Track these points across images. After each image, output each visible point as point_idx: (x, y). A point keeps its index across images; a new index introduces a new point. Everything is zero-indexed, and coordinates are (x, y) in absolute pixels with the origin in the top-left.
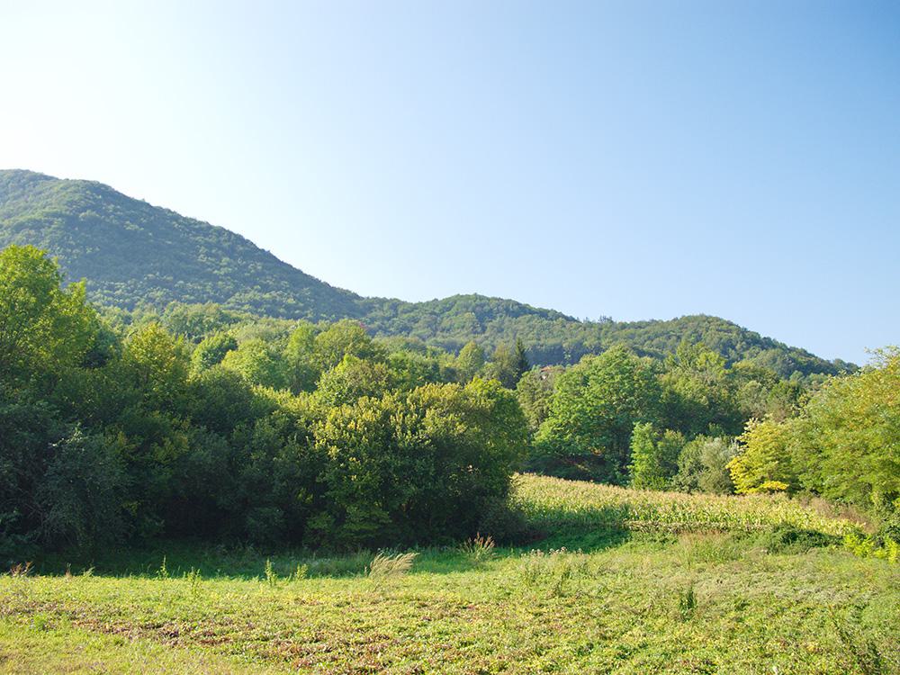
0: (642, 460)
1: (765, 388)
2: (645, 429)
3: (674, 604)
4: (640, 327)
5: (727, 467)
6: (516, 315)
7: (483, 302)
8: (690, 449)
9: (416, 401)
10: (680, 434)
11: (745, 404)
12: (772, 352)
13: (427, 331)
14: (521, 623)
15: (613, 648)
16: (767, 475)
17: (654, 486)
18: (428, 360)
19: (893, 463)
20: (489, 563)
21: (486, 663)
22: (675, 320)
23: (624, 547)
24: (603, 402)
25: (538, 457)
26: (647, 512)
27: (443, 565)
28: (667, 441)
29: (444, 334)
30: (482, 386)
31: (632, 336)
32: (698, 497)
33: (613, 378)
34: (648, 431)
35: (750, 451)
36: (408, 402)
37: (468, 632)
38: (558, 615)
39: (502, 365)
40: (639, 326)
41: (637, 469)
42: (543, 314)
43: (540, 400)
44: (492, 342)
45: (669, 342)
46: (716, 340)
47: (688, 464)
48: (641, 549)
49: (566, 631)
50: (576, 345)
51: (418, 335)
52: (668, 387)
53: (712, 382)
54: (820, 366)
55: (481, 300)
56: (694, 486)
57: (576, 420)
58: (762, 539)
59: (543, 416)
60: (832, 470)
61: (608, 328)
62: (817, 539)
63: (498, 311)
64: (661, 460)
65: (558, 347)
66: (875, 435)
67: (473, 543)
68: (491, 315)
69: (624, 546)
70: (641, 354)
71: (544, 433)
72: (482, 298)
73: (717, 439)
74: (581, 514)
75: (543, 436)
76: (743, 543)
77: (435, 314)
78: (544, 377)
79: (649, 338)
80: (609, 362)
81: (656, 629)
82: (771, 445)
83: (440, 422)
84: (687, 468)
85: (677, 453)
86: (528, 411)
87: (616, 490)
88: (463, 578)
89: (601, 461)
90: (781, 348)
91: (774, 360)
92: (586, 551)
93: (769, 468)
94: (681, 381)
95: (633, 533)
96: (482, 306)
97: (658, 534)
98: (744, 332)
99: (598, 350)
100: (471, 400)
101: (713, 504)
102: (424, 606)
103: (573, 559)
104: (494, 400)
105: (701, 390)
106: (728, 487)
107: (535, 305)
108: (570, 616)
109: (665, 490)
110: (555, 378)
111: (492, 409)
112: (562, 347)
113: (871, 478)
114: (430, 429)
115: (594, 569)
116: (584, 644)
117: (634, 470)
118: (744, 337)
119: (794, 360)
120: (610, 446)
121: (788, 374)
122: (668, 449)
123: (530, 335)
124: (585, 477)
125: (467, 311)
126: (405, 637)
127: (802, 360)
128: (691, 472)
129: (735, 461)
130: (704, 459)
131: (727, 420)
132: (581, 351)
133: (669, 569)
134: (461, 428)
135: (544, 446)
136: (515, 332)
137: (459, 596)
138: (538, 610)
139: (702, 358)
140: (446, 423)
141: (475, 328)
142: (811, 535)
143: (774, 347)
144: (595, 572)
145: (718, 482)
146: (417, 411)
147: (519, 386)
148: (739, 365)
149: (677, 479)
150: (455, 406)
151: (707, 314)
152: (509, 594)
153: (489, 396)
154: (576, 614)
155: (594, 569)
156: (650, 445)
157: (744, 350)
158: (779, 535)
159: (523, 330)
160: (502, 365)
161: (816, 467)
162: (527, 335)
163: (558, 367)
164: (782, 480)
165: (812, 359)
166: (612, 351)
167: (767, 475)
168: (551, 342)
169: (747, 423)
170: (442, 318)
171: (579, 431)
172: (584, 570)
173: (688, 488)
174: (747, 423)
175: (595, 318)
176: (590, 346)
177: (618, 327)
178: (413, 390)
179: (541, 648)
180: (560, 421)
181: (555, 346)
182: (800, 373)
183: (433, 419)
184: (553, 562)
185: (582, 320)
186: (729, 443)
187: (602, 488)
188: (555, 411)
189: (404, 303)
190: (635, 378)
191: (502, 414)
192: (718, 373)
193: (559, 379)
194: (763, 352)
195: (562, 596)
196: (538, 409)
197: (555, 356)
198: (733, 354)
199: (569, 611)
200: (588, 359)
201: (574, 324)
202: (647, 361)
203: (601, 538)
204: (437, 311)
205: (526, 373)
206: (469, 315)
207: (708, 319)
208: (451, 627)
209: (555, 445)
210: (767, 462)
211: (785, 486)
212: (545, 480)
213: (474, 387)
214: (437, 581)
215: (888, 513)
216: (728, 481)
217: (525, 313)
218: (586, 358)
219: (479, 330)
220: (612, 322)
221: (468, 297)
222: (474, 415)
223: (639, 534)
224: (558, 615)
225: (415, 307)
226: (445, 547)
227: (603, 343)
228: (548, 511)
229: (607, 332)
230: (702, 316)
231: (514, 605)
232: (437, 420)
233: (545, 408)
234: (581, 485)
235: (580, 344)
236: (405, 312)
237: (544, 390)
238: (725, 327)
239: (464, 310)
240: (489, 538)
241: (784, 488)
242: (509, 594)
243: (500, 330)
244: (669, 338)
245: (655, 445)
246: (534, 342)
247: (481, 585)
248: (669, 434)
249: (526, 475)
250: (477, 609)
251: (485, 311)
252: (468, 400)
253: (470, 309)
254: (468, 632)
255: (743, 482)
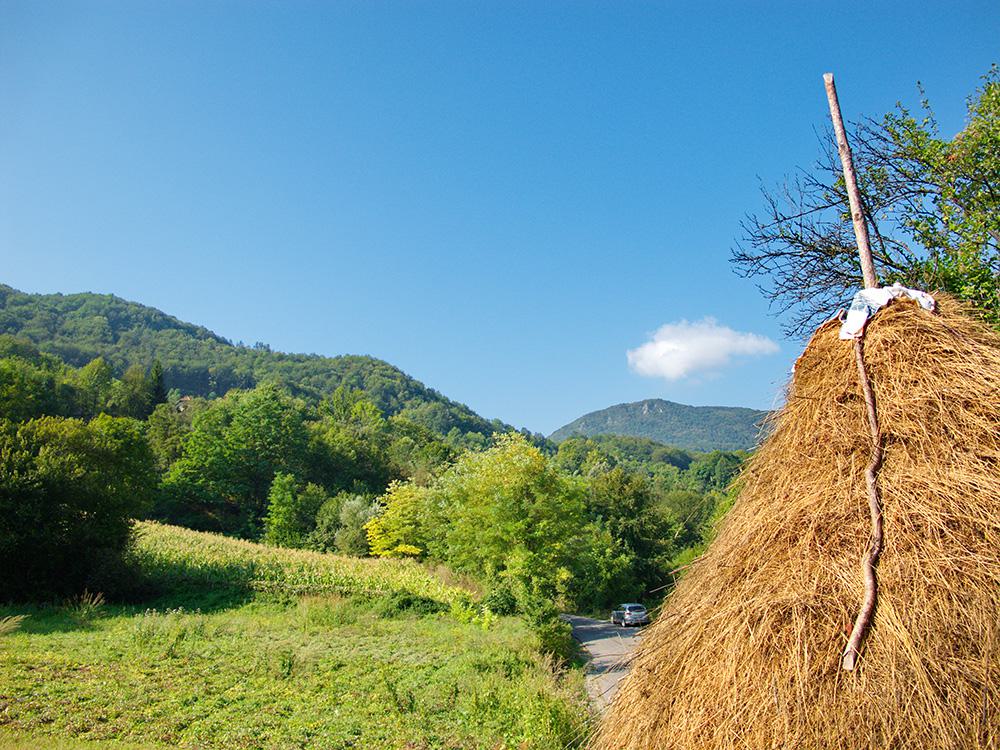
0: (278, 513)
1: (417, 446)
2: (286, 479)
3: (277, 665)
4: (299, 361)
5: (364, 527)
6: (158, 327)
7: (120, 306)
8: (330, 505)
9: (28, 435)
10: (322, 489)
11: (396, 461)
12: (434, 405)
13: (44, 332)
14: (134, 682)
15: (215, 700)
16: (402, 538)
17: (289, 542)
18: (42, 373)
19: (502, 540)
20: (98, 622)
21: (105, 712)
22: (337, 358)
23: (245, 609)
24: (244, 446)
25: (164, 501)
26: (274, 573)
27: (43, 625)
28: (308, 495)
29: (65, 338)
30: (109, 424)
31: (289, 370)
32: (331, 558)
33: (259, 421)
34: (288, 482)
35: (388, 513)
36: (19, 434)
37: (83, 690)
38: (169, 675)
39: (133, 389)
40: (298, 359)
41: (272, 522)
42: (191, 330)
43: (174, 437)
44: (125, 355)
45: (329, 382)
46: (378, 385)
47: (326, 521)
48: (263, 610)
49: (175, 688)
50: (225, 371)
51: (29, 335)
52: (317, 437)
53: (364, 435)
54: (479, 424)
55: (117, 303)
56: (330, 545)
57: (212, 464)
58: (380, 604)
59: (176, 455)
60: (455, 540)
61: (264, 356)
62: (430, 606)
63: (137, 320)
64: (299, 514)
65: (203, 371)
66: (491, 512)
67: (80, 600)
68: (127, 322)
69: (245, 607)
70: (296, 392)
71: (174, 474)
72: (118, 301)
73: (359, 497)
74: (205, 570)
75: (172, 478)
76: (361, 608)
77: (56, 311)
78: (182, 409)
79: (307, 377)
80: (258, 402)
81: (256, 685)
82: (409, 509)
83: (55, 463)
84: (325, 525)
85: (317, 509)
86: (159, 448)
87: (245, 544)
88: (71, 638)
89: (234, 510)
90: (443, 401)
91: (435, 414)
92: (205, 611)
93: (405, 532)
94: (331, 431)
95: (257, 594)
96: (118, 311)
97: (282, 596)
98: (407, 380)
99: (250, 384)
100: (96, 440)
101: (342, 566)
102: (31, 668)
103: (191, 620)
104: (122, 441)
105: (351, 444)
106: (362, 548)
107: (183, 318)
108: (180, 676)
109: (300, 547)
110: (192, 411)
111: (118, 451)
112: (207, 371)
113: (481, 552)
114: (42, 470)
115: (211, 629)
116: (190, 698)
117: (270, 523)
118: (408, 385)
119: (454, 416)
120: (247, 496)
121: (446, 429)
122: (307, 503)
123: (172, 353)
124: (214, 528)
125: (98, 314)
126: (23, 696)
127: (463, 416)
128: (329, 529)
129: (373, 521)
130: (343, 517)
131: (371, 475)
132: (229, 379)
133: (285, 632)
134: (79, 471)
135: (172, 489)
136: (154, 347)
137: (67, 659)
138: (150, 671)
139: (357, 407)
140: (63, 463)
141: (105, 335)
142: (424, 602)
143: (437, 400)
144: (211, 634)
145: (355, 542)
146: (28, 447)
147: (152, 419)
148: (397, 418)
149: (314, 535)
150: (75, 445)
151: (373, 356)
152: (121, 655)
153: (116, 436)
154: (187, 674)
155: (211, 629)
156: (289, 497)
157: (406, 400)
158: (396, 602)
159: (164, 346)
160: (133, 389)
161: (443, 536)
162: (168, 352)
163: (199, 399)
164: (416, 545)
165: (472, 417)
166: (260, 392)
167: (402, 538)
168: (196, 364)
169: (390, 485)
170: (64, 318)
171: (214, 476)
172: (200, 631)
173: (323, 546)
174: (390, 485)
175: (250, 343)
176: (241, 374)
177: (276, 356)
178: (26, 422)
179: (152, 701)
180: (194, 463)
181: (199, 369)
182: (458, 430)
183: (47, 458)
184: (168, 623)
185: (234, 343)
186: (370, 504)
187: (231, 541)
188: (190, 451)
189: (16, 292)
190: (283, 424)
191: (133, 456)
192: (372, 425)
193: (198, 417)
194: (424, 404)
195: (175, 657)
196: (170, 448)
197: (200, 384)
198: (394, 402)
199: (180, 671)
200: (235, 395)
201: (225, 348)
202: (300, 403)
203: (223, 597)
204: (59, 309)
205: (161, 405)
206: (99, 319)
207: (373, 362)
208: (67, 687)
209: (185, 489)
210: (404, 525)
211: (417, 551)
212: (169, 530)
213: (100, 424)
214: (37, 642)
215: (497, 583)
216: (362, 541)
217: (169, 327)
218: (231, 394)
219: (110, 339)
220: (269, 351)
221: (101, 297)
222: (97, 457)
223: (262, 595)
224: (169, 675)
225: (29, 300)
226: (45, 603)
227: (256, 373)
228: (169, 565)
229: (263, 361)
230: (367, 357)
231: (127, 666)
232: (52, 461)
233: (178, 447)
234: (209, 537)
235: (228, 371)
236: (15, 303)
237: (180, 424)
238: (389, 372)
239: (94, 312)
240: (99, 596)
241: (417, 553)
242: (121, 655)
243: (136, 343)
244: (329, 376)
245: (295, 498)
246: (176, 361)
247: (89, 647)
248: (310, 487)
249: (147, 523)
250: (89, 670)
251: (120, 318)
252: (91, 439)
253: (102, 312)
254: (83, 690)
255: (378, 544)
